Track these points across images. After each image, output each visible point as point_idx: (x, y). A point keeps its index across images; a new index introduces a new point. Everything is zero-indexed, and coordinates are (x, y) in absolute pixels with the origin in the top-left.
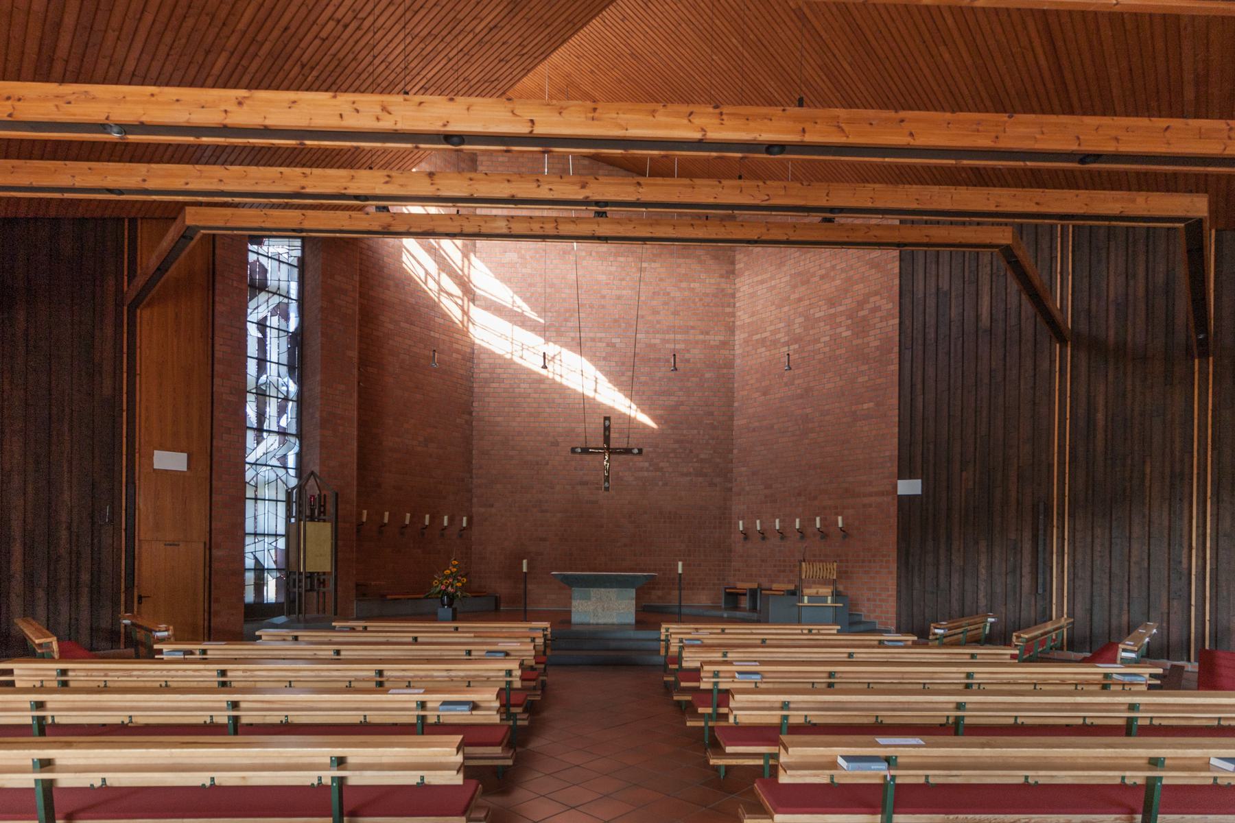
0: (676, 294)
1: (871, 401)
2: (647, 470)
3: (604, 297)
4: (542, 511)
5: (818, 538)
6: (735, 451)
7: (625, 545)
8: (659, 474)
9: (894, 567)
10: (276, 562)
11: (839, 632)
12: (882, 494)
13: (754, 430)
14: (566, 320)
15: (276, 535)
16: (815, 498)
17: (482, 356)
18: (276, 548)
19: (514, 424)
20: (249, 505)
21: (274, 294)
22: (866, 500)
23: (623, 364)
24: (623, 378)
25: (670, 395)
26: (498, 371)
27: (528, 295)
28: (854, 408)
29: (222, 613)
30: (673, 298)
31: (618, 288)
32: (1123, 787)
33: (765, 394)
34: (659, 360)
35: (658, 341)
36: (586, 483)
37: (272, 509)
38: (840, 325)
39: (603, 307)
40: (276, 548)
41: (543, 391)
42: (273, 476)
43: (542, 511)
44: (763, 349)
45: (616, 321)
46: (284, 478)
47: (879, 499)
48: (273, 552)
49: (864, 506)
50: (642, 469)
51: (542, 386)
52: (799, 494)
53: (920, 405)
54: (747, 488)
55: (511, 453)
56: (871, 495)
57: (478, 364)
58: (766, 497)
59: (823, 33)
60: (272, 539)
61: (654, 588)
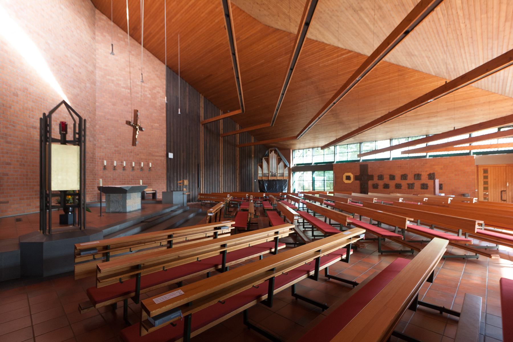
1: (158, 123)
5: (139, 170)
6: (97, 127)
9: (165, 181)
11: (236, 231)
12: (161, 156)
13: (108, 119)
16: (138, 155)
19: (186, 182)
21: (130, 62)
22: (157, 158)
28: (152, 124)
29: (494, 167)
32: (267, 243)
33: (114, 105)
38: (146, 91)
44: (113, 85)
47: (161, 158)
49: (156, 160)
52: (131, 152)
53: (172, 130)
54: (105, 146)
56: (156, 156)
58: (115, 151)
59: (175, 19)
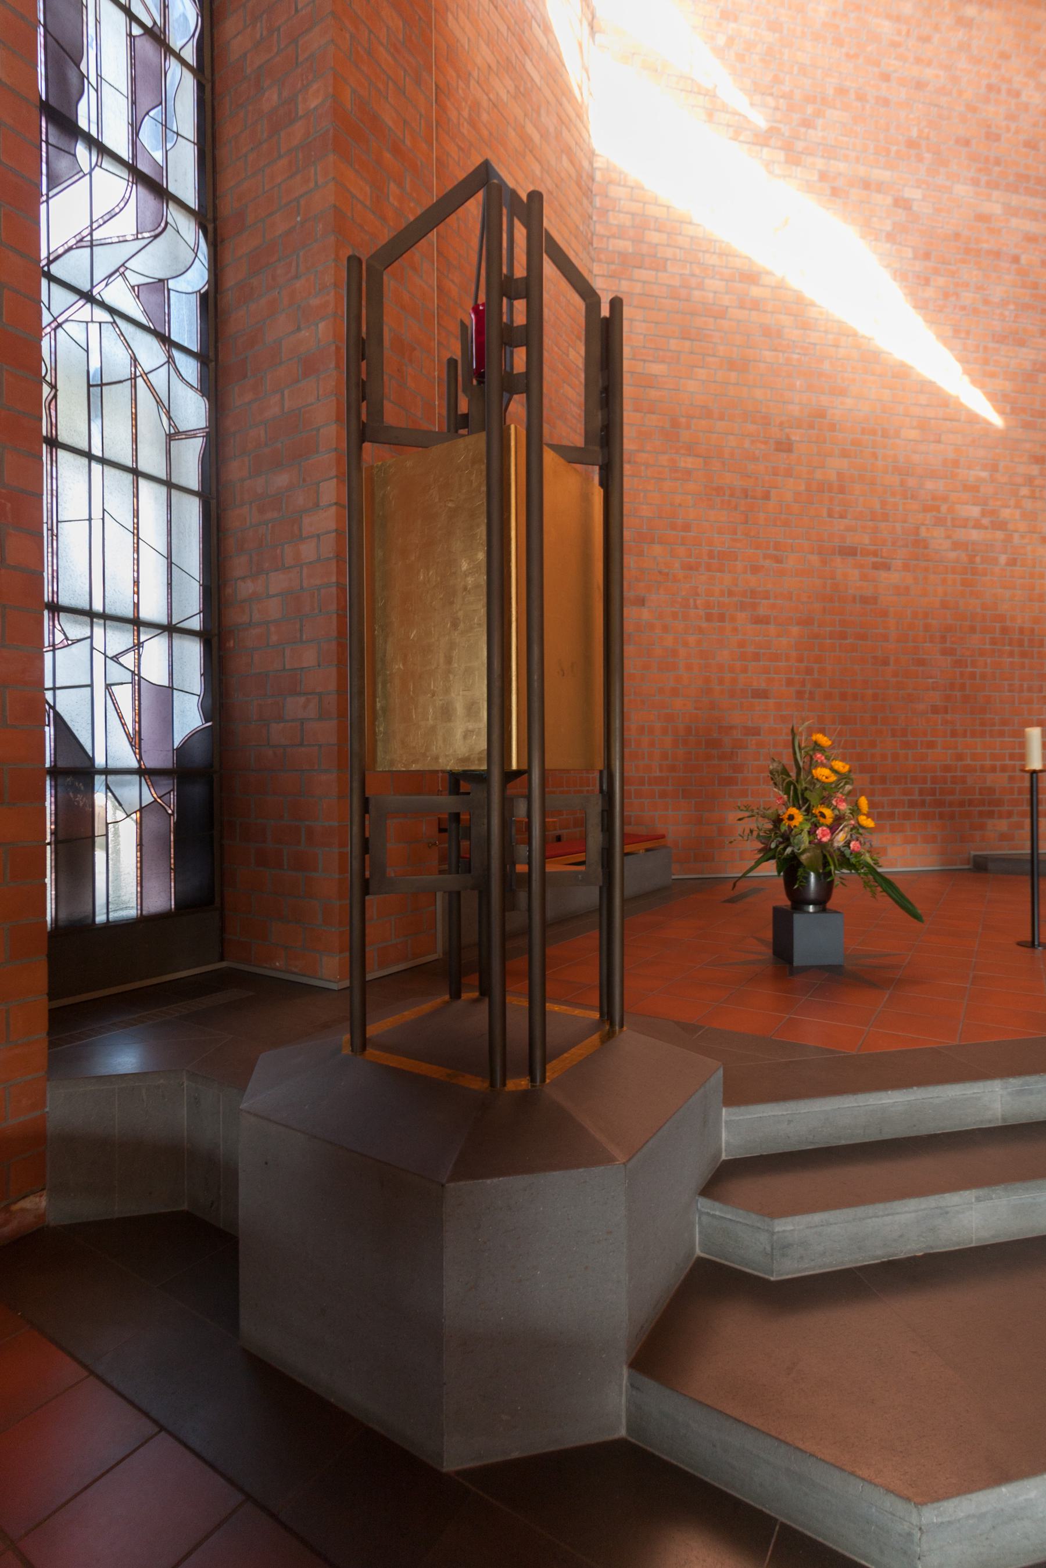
0: (1032, 96)
2: (977, 525)
3: (886, 77)
4: (758, 620)
7: (935, 710)
8: (1000, 535)
10: (136, 741)
14: (807, 124)
15: (136, 623)
17: (614, 191)
18: (137, 679)
20: (48, 657)
23: (927, 256)
24: (929, 293)
25: (1022, 343)
26: (654, 237)
27: (721, 40)
30: (1026, 107)
31: (918, 61)
34: (997, 255)
35: (997, 209)
36: (850, 552)
37: (119, 504)
39: (886, 102)
40: (137, 679)
41: (756, 305)
42: (118, 364)
43: (758, 620)
45: (911, 144)
46: (159, 379)
48: (124, 695)
50: (964, 523)
51: (755, 291)
55: (687, 462)
57: (604, 212)
60: (119, 639)
61: (990, 814)
